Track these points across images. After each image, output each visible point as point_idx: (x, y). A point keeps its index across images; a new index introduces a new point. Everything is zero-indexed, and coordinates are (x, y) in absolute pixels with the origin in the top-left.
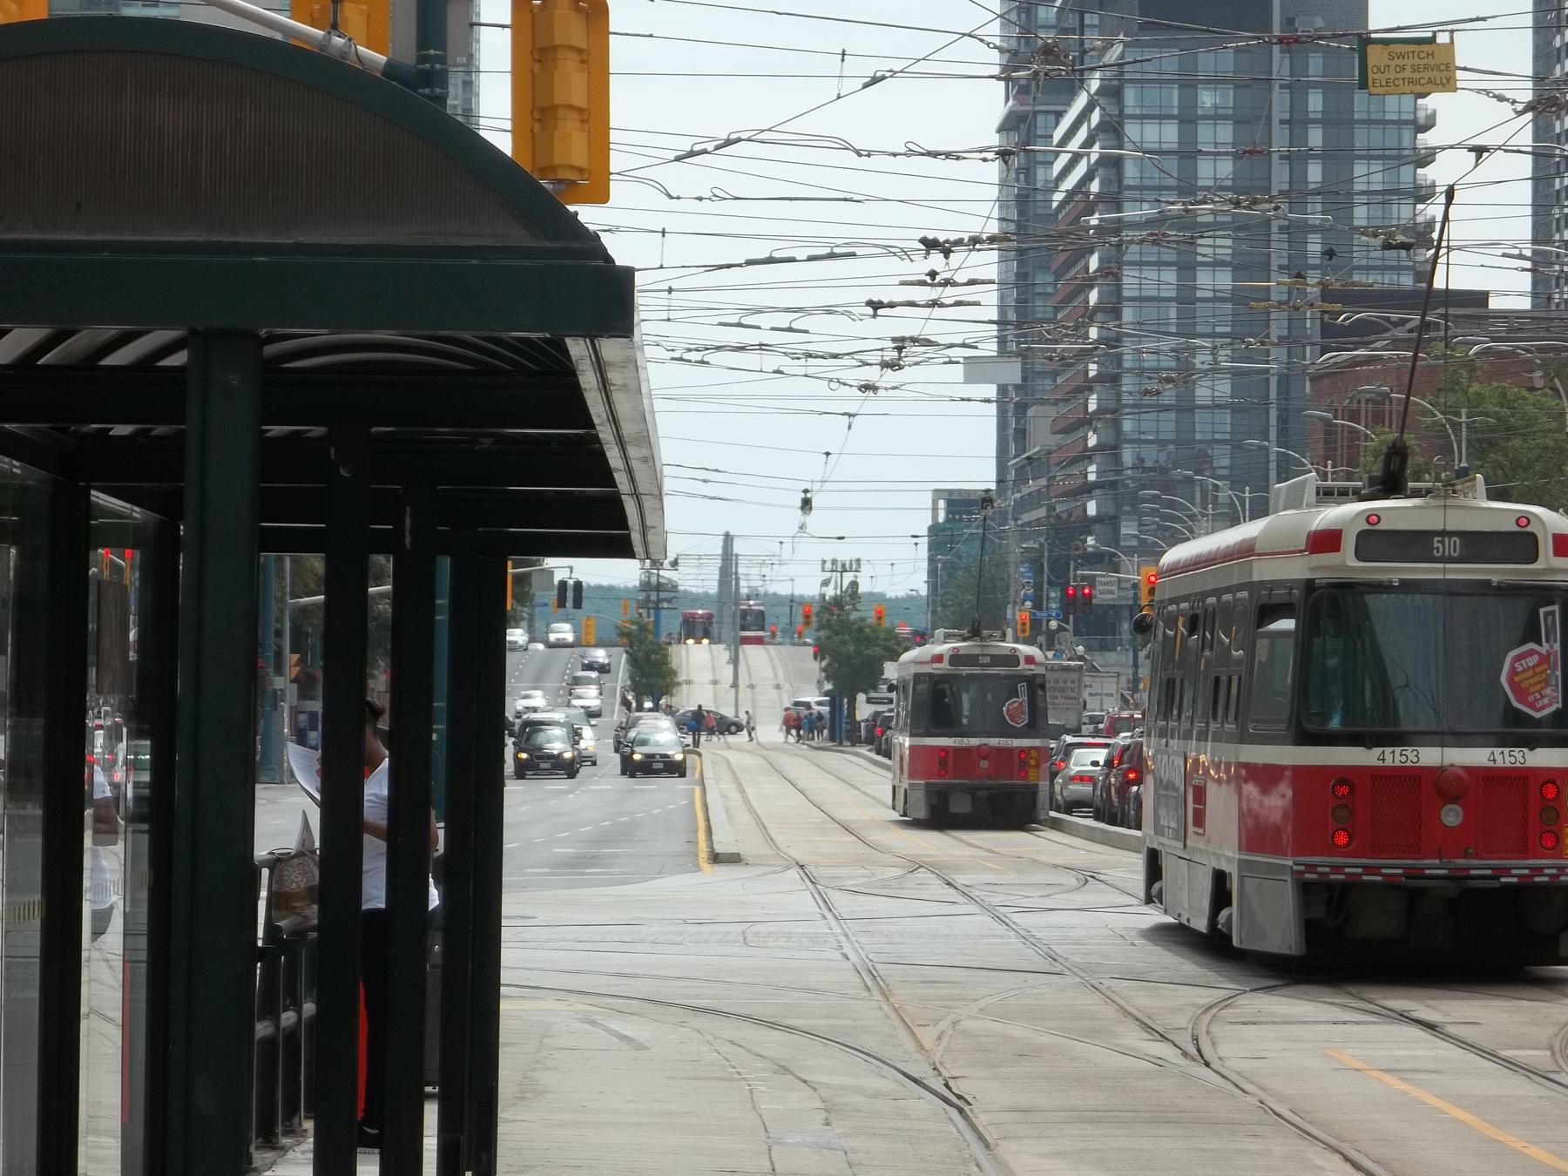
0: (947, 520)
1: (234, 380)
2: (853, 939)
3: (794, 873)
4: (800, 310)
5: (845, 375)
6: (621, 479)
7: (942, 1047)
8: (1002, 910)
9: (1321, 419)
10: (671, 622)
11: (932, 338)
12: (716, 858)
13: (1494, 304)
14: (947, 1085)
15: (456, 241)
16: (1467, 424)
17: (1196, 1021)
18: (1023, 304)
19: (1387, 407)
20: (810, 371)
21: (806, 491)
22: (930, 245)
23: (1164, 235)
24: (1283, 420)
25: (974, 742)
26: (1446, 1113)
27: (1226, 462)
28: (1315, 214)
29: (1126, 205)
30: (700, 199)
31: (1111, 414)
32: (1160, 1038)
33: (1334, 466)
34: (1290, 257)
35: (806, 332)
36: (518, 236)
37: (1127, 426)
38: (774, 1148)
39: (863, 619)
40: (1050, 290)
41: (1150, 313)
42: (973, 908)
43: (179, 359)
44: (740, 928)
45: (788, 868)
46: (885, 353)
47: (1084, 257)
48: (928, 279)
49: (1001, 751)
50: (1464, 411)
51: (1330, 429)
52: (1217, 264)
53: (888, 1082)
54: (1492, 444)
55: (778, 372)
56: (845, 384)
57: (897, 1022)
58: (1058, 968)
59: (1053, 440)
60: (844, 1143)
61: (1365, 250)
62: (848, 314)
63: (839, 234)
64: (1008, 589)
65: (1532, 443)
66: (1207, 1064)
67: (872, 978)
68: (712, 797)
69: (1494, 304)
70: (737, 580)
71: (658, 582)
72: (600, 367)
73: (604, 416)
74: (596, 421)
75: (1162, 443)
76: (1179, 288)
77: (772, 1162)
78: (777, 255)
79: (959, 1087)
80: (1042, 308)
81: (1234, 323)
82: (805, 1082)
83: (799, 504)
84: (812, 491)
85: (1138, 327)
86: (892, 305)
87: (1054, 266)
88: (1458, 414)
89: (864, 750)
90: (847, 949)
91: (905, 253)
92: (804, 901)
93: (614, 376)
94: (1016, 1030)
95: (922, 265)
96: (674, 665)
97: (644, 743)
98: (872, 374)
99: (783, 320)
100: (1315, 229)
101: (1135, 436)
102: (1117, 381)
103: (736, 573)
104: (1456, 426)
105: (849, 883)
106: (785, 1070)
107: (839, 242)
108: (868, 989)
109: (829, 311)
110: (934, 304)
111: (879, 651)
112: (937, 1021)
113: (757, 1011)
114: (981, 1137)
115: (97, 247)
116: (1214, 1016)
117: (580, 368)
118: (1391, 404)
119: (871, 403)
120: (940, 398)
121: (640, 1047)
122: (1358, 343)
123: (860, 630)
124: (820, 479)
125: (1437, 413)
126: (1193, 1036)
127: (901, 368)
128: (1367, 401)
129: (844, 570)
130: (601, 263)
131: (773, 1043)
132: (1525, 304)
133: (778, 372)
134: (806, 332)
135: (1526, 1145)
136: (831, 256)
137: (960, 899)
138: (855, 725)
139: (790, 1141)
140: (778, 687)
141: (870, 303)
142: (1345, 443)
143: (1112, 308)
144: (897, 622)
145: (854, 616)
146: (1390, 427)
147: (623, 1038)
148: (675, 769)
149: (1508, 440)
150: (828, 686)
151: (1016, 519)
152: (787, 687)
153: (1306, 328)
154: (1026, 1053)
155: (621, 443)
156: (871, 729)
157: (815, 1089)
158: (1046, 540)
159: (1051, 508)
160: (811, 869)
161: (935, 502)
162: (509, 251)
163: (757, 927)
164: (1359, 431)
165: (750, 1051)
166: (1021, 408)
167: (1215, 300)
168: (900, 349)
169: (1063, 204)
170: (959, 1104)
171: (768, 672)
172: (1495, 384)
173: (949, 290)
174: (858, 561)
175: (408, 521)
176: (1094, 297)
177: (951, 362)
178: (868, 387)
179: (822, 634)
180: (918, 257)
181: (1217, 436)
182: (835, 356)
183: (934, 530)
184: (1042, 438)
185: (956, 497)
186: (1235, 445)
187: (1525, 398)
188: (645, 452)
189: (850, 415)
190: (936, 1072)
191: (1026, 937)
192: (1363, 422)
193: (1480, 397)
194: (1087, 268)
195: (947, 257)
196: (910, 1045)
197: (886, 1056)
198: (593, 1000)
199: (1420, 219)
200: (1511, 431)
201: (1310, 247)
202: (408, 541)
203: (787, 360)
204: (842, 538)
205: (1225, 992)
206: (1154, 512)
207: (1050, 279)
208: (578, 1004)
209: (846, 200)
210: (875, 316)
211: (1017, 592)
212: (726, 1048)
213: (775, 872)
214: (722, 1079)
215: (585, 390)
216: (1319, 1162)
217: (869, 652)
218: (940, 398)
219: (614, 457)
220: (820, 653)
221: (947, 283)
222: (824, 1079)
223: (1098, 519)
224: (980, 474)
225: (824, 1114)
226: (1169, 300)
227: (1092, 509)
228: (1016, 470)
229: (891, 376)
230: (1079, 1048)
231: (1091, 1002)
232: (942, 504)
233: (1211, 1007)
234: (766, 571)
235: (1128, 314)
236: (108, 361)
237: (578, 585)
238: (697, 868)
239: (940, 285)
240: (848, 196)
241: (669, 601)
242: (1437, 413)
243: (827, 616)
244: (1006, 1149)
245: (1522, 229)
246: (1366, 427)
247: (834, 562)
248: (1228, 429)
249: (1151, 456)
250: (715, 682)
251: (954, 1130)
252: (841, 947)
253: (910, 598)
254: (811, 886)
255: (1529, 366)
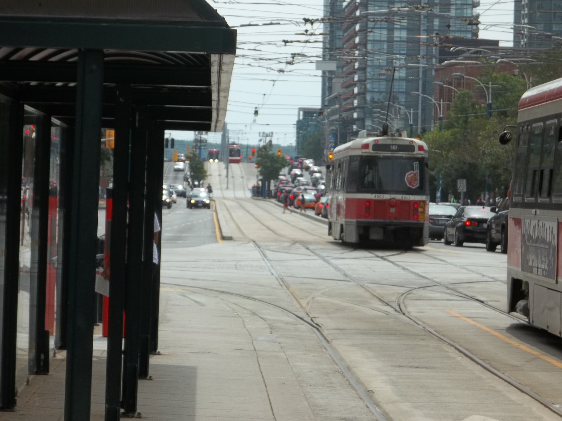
0: (304, 119)
1: (94, 67)
2: (274, 267)
3: (252, 244)
4: (259, 43)
5: (273, 67)
6: (214, 104)
7: (309, 307)
8: (327, 258)
9: (439, 85)
10: (205, 154)
11: (306, 54)
12: (224, 238)
13: (501, 45)
14: (312, 320)
15: (174, 19)
16: (492, 88)
17: (399, 299)
18: (332, 41)
19: (462, 81)
20: (261, 65)
21: (256, 108)
22: (306, 20)
23: (390, 19)
24: (424, 85)
25: (387, 197)
26: (490, 333)
27: (403, 100)
28: (436, 11)
29: (370, 8)
30: (225, 3)
31: (362, 81)
32: (386, 304)
33: (443, 101)
34: (428, 26)
35: (260, 51)
36: (196, 18)
37: (369, 86)
38: (254, 342)
39: (273, 154)
40: (341, 37)
41: (377, 46)
42: (316, 257)
43: (75, 59)
44: (234, 263)
45: (249, 242)
46: (287, 59)
47: (354, 25)
48: (305, 33)
49: (402, 202)
50: (490, 83)
51: (441, 87)
52: (401, 29)
53: (291, 319)
54: (500, 95)
55: (249, 65)
56: (273, 70)
57: (293, 298)
58: (348, 279)
59: (342, 91)
60: (279, 340)
61: (455, 25)
62: (276, 44)
63: (274, 17)
64: (325, 143)
65: (514, 95)
66: (404, 314)
67: (283, 282)
68: (220, 216)
69: (501, 45)
70: (228, 139)
71: (200, 139)
72: (220, 64)
73: (216, 82)
74: (212, 83)
75: (380, 92)
76: (388, 37)
77: (254, 347)
78: (252, 23)
79: (317, 321)
80: (338, 43)
81: (407, 50)
82: (262, 318)
83: (253, 112)
84: (258, 108)
85: (379, 51)
86: (291, 42)
87: (344, 28)
88: (488, 84)
89: (274, 200)
90: (273, 271)
91: (297, 23)
92: (256, 254)
93: (224, 68)
94: (335, 301)
95: (303, 28)
96: (205, 168)
97: (196, 196)
98: (283, 66)
99: (253, 46)
100: (437, 16)
101: (371, 90)
102: (365, 70)
103: (228, 136)
104: (488, 88)
105: (272, 248)
106: (254, 314)
107: (274, 19)
108: (281, 285)
109: (269, 43)
110: (307, 42)
111: (279, 165)
112: (307, 297)
113: (242, 293)
114: (325, 339)
115: (46, 19)
116: (405, 297)
117: (213, 64)
118: (464, 79)
119: (282, 77)
120: (306, 75)
121: (202, 305)
122: (452, 58)
123: (273, 158)
124: (261, 103)
125: (481, 83)
126: (398, 304)
127: (293, 64)
128: (455, 79)
129: (267, 136)
130: (225, 28)
131: (249, 304)
132: (511, 45)
133: (249, 65)
134: (260, 51)
135: (520, 344)
136: (271, 24)
137: (311, 254)
138: (270, 191)
139: (259, 339)
140: (242, 177)
141: (284, 41)
142: (447, 94)
143: (364, 43)
144: (285, 155)
145: (270, 153)
146: (463, 88)
147: (196, 302)
148: (206, 206)
149: (506, 93)
150: (261, 177)
151: (328, 119)
152: (246, 177)
153: (432, 52)
154: (339, 309)
155: (219, 91)
156: (276, 193)
157: (265, 321)
158: (339, 126)
159: (341, 115)
160: (258, 243)
161: (299, 113)
162: (192, 23)
163: (240, 263)
164: (452, 89)
165: (241, 307)
166: (330, 79)
167: (401, 41)
168: (293, 58)
169: (346, 7)
170: (317, 327)
171: (239, 172)
172: (502, 73)
173: (313, 37)
174: (272, 133)
175: (137, 117)
176: (357, 40)
177: (311, 62)
178: (281, 71)
179: (259, 159)
180: (302, 25)
181: (401, 90)
182: (270, 60)
183: (299, 122)
184: (338, 89)
185: (306, 110)
186: (407, 93)
187: (512, 79)
188: (226, 94)
189: (274, 81)
190: (307, 315)
191: (336, 268)
192: (453, 85)
193: (496, 78)
194: (355, 29)
195: (312, 25)
196: (297, 306)
197: (289, 309)
198: (187, 288)
199: (474, 14)
200: (507, 90)
201: (435, 23)
202: (137, 124)
203: (253, 61)
204: (268, 125)
205: (408, 289)
206: (378, 117)
207: (341, 33)
208: (179, 290)
209: (277, 4)
210: (285, 45)
211: (328, 145)
212: (233, 306)
213: (245, 243)
214: (233, 317)
215: (212, 72)
216: (446, 349)
217: (276, 165)
218: (306, 75)
219: (214, 96)
220: (259, 164)
221: (312, 34)
222: (269, 317)
223: (358, 119)
224: (316, 103)
225: (270, 330)
226: (384, 41)
227: (355, 115)
228: (328, 101)
229: (290, 67)
230: (357, 307)
231: (360, 291)
232: (301, 113)
233: (403, 294)
234: (240, 136)
235: (369, 47)
236: (14, 58)
237: (173, 140)
238: (216, 241)
239: (309, 35)
240: (278, 3)
241: (204, 146)
242: (481, 83)
243: (260, 152)
244: (335, 343)
245: (511, 19)
246: (455, 87)
247: (264, 133)
248: (404, 87)
249: (377, 97)
250: (220, 175)
251: (315, 336)
252: (270, 271)
253: (289, 147)
254: (258, 249)
255: (514, 67)
